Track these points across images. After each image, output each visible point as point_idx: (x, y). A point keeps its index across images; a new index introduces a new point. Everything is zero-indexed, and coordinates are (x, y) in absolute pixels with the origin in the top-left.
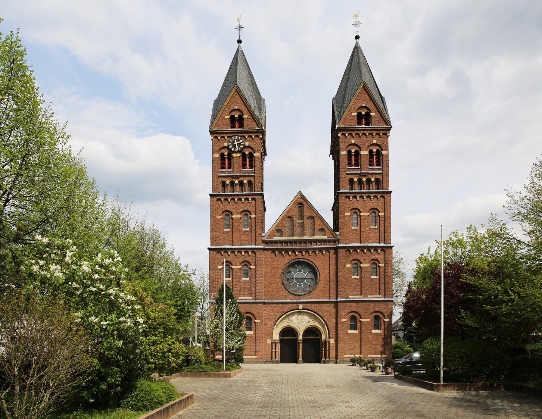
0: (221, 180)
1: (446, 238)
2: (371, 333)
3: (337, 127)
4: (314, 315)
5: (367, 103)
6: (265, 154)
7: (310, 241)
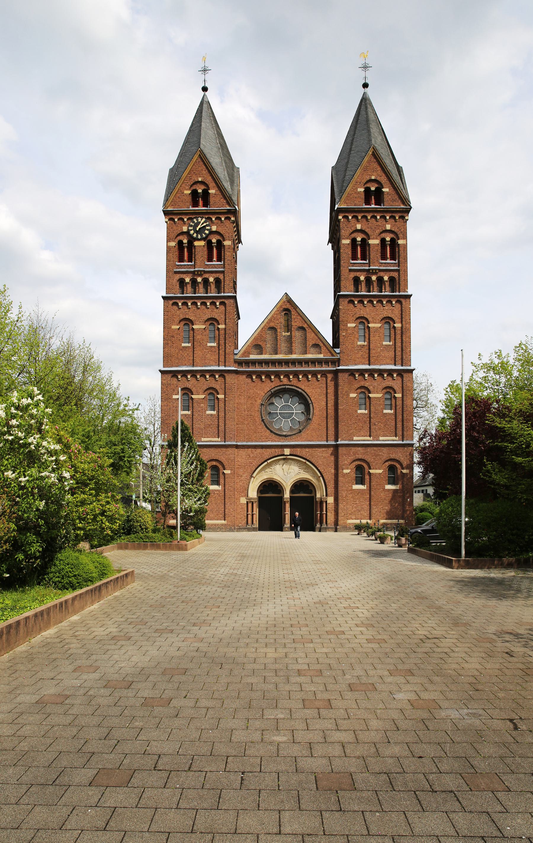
0: (178, 277)
1: (486, 360)
2: (384, 489)
3: (337, 206)
4: (306, 463)
5: (378, 175)
6: (240, 241)
7: (300, 362)
